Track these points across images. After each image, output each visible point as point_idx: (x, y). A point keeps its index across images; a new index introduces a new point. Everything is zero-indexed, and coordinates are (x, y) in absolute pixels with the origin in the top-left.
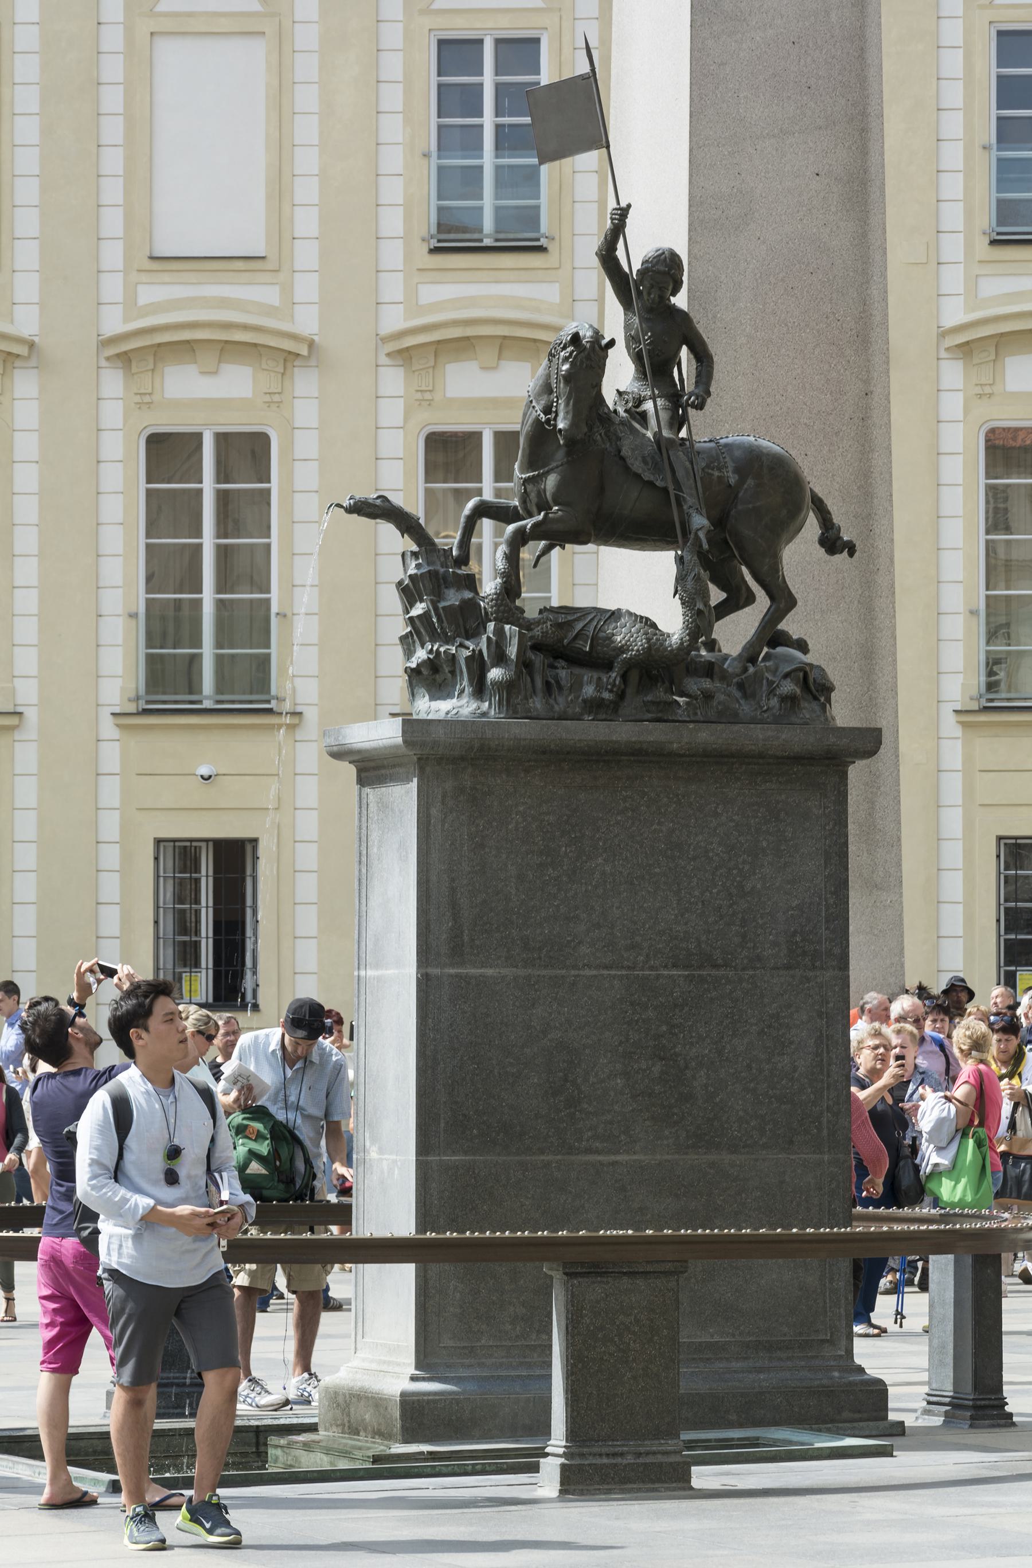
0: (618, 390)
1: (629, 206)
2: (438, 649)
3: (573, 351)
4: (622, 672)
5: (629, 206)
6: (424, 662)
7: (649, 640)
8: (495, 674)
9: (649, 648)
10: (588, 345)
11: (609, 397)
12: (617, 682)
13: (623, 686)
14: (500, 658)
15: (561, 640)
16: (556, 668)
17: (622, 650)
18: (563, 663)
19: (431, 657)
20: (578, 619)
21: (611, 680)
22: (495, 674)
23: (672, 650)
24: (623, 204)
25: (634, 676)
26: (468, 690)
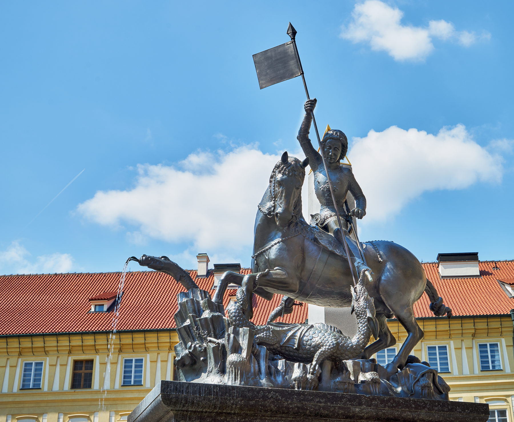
0: (311, 215)
1: (315, 100)
2: (195, 346)
3: (284, 167)
4: (320, 362)
5: (315, 100)
6: (187, 355)
7: (337, 339)
8: (232, 357)
9: (338, 344)
10: (293, 163)
11: (308, 220)
12: (317, 368)
13: (320, 371)
14: (237, 349)
15: (279, 342)
16: (276, 359)
17: (318, 347)
18: (280, 357)
19: (191, 351)
20: (289, 330)
21: (312, 366)
22: (232, 357)
23: (352, 346)
24: (312, 98)
25: (328, 365)
26: (215, 370)
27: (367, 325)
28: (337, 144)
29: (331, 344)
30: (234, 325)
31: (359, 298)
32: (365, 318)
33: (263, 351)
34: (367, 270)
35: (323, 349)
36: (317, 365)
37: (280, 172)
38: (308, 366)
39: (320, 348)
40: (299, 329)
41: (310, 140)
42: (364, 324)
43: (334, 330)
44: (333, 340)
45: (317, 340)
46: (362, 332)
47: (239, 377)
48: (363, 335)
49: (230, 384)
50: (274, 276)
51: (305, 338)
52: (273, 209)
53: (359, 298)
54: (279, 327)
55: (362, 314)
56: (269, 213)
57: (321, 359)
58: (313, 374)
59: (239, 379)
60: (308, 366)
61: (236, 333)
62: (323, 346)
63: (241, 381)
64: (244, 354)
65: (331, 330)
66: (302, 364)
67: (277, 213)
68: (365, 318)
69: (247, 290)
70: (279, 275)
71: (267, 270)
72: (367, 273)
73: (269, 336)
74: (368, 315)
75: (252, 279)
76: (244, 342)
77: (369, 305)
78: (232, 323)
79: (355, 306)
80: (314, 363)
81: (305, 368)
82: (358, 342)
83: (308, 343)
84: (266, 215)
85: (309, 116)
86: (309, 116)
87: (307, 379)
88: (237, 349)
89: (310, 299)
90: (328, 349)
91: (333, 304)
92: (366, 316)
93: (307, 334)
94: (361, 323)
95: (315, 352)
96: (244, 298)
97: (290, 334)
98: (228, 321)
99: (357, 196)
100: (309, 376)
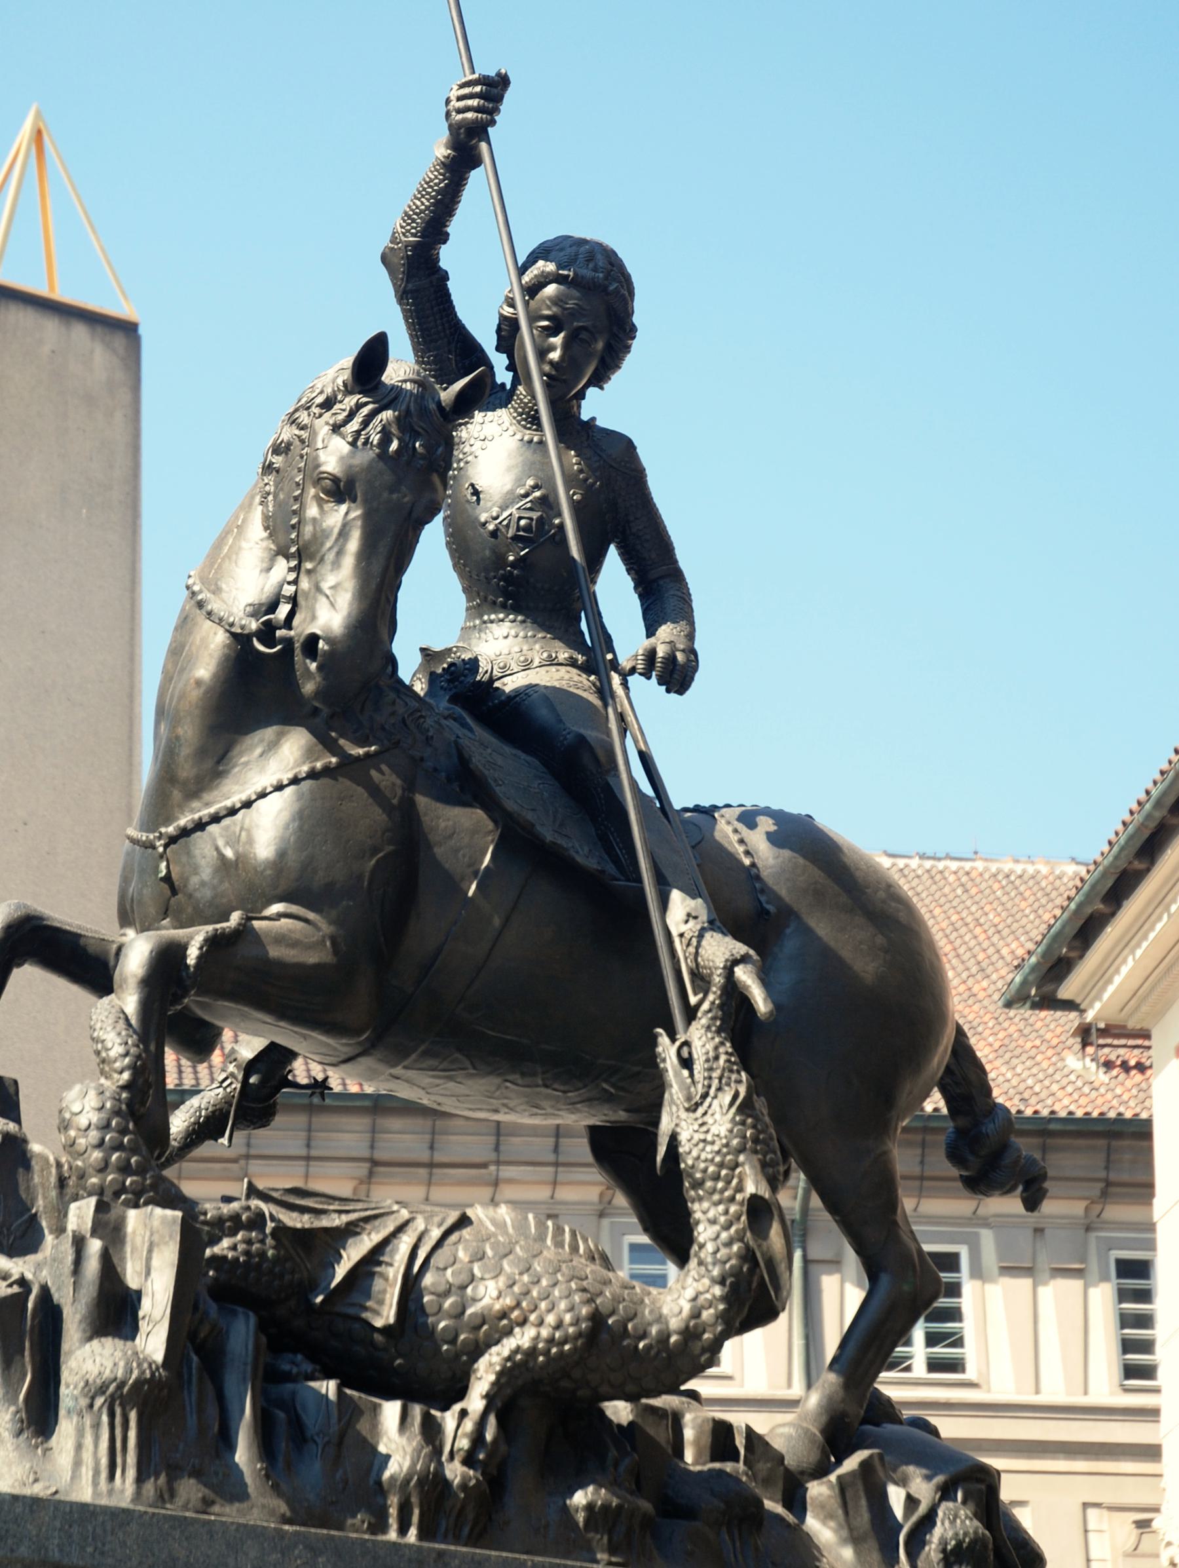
3: (359, 406)
11: (409, 668)
12: (489, 1437)
17: (498, 1326)
21: (469, 1425)
22: (88, 1360)
23: (664, 1337)
27: (740, 1237)
28: (592, 307)
29: (568, 1318)
30: (100, 1191)
31: (705, 1096)
32: (732, 1199)
33: (242, 1335)
34: (744, 959)
35: (523, 1338)
36: (492, 1420)
37: (336, 428)
38: (449, 1420)
39: (509, 1332)
40: (401, 1229)
41: (445, 276)
42: (727, 1227)
43: (574, 1248)
44: (577, 1298)
45: (488, 1295)
46: (716, 1272)
47: (132, 1458)
48: (722, 1282)
49: (85, 1494)
50: (274, 952)
51: (428, 1280)
52: (283, 610)
53: (705, 1096)
54: (303, 1210)
55: (716, 1178)
56: (267, 633)
57: (509, 1391)
58: (469, 1460)
59: (131, 1473)
60: (449, 1420)
61: (109, 1229)
62: (523, 1322)
63: (140, 1480)
64: (153, 1342)
65: (559, 1244)
66: (417, 1410)
67: (313, 639)
68: (732, 1199)
69: (145, 1007)
70: (295, 944)
71: (235, 918)
72: (743, 974)
73: (262, 1254)
74: (750, 1188)
75: (167, 960)
76: (156, 1285)
77: (756, 1140)
78: (82, 1176)
79: (683, 1137)
80: (475, 1402)
81: (431, 1431)
82: (696, 1314)
83: (447, 1304)
84: (240, 640)
85: (466, 149)
86: (466, 149)
87: (447, 1483)
88: (116, 1311)
89: (410, 1074)
90: (551, 1341)
91: (512, 1104)
92: (740, 1189)
93: (439, 1259)
94: (713, 1222)
95: (477, 1350)
96: (138, 1057)
97: (353, 1253)
98: (59, 1165)
99: (653, 575)
100: (455, 1471)
